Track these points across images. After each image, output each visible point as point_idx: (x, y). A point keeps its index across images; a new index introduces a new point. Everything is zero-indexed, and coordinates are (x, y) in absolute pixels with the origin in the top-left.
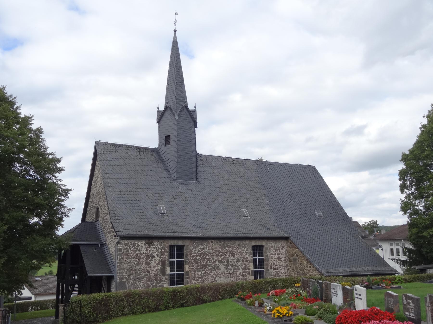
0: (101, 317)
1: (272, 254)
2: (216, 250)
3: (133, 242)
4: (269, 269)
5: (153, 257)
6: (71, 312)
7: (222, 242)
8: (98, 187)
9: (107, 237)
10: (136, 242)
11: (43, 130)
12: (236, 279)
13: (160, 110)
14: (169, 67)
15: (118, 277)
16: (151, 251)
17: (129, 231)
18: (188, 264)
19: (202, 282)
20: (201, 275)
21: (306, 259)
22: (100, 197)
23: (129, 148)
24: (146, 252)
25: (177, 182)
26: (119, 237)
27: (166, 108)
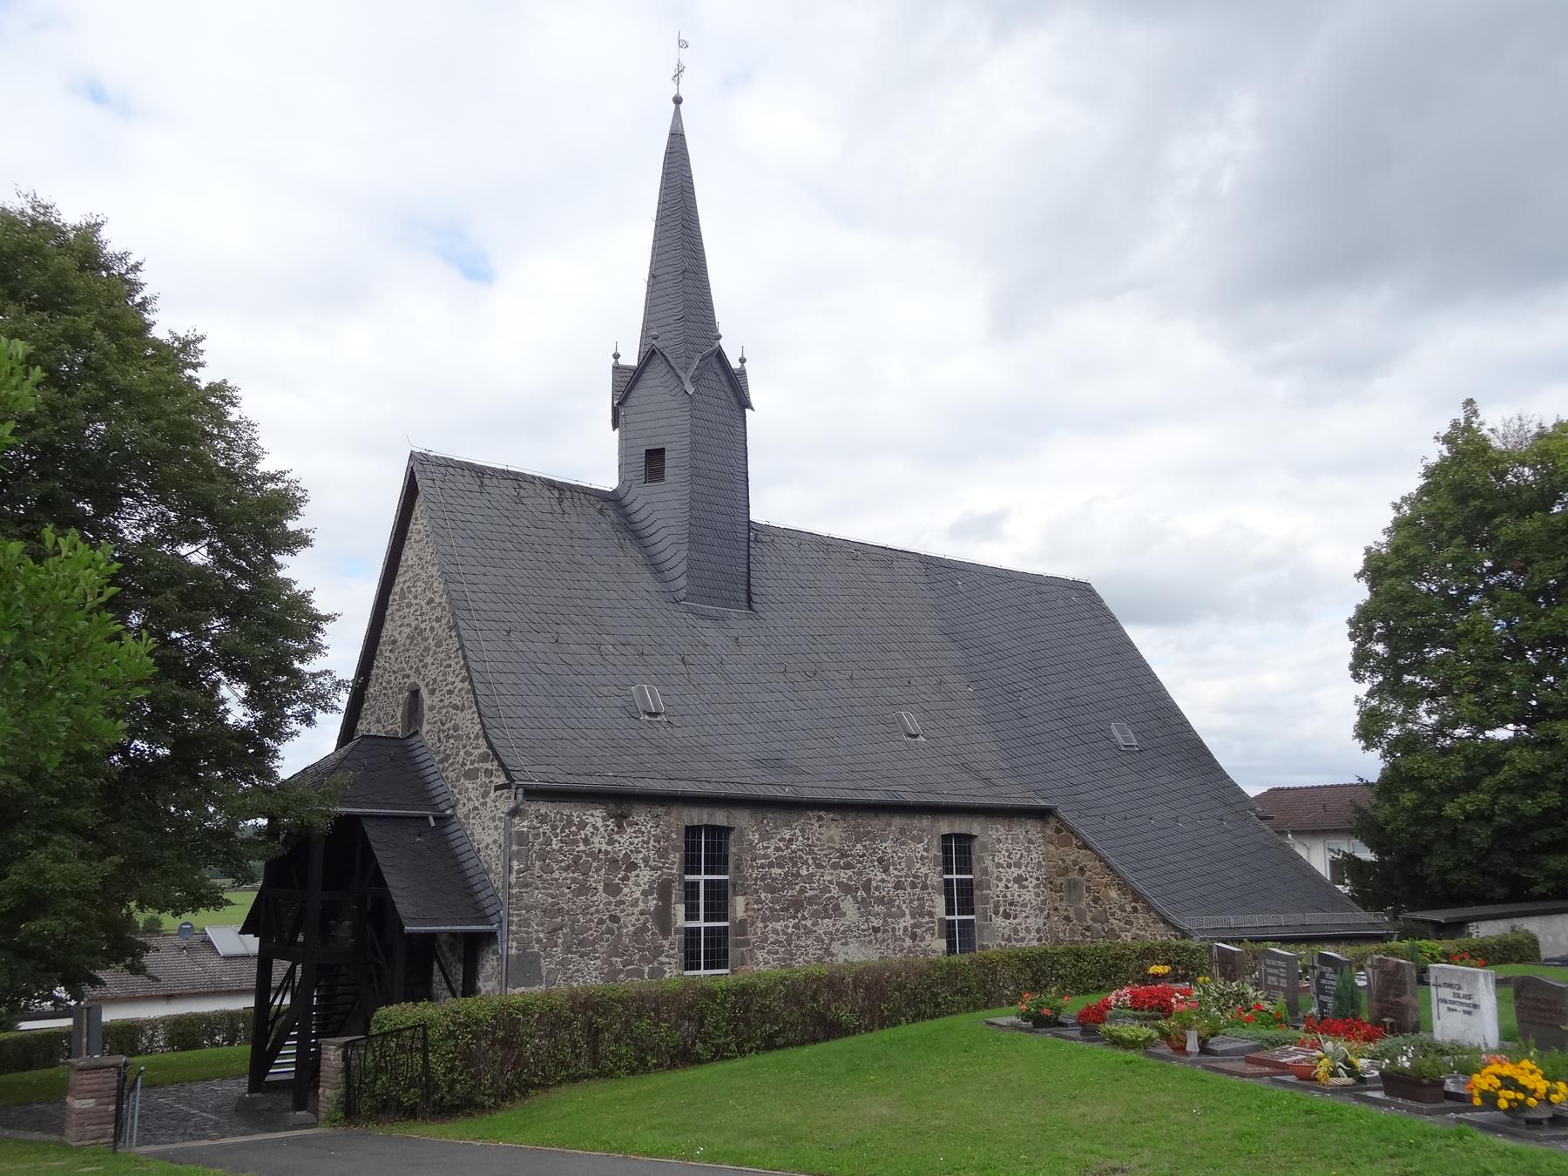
0: (490, 1091)
1: (999, 865)
2: (833, 848)
3: (567, 809)
5: (633, 866)
6: (379, 1070)
7: (851, 820)
8: (418, 613)
9: (460, 793)
10: (573, 811)
11: (235, 394)
12: (894, 950)
13: (622, 362)
14: (657, 219)
15: (511, 936)
16: (626, 846)
17: (552, 768)
19: (786, 958)
20: (785, 933)
21: (1118, 884)
22: (427, 649)
23: (523, 484)
24: (609, 848)
25: (689, 610)
26: (521, 790)
27: (649, 355)
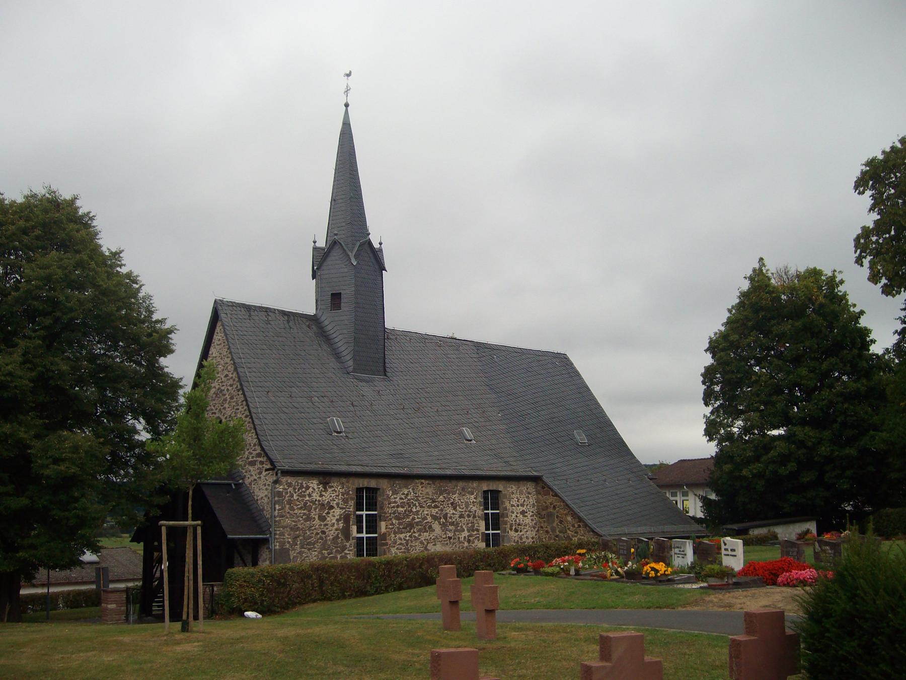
1: (513, 506)
3: (300, 480)
4: (508, 531)
5: (332, 507)
8: (219, 381)
13: (318, 245)
17: (293, 461)
18: (386, 520)
20: (405, 540)
22: (225, 400)
23: (270, 313)
